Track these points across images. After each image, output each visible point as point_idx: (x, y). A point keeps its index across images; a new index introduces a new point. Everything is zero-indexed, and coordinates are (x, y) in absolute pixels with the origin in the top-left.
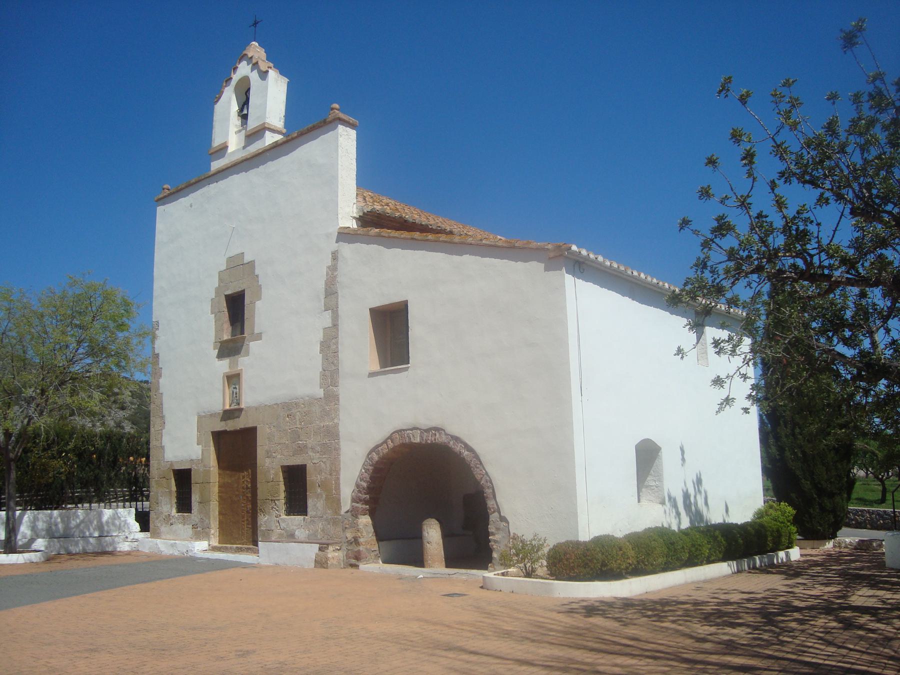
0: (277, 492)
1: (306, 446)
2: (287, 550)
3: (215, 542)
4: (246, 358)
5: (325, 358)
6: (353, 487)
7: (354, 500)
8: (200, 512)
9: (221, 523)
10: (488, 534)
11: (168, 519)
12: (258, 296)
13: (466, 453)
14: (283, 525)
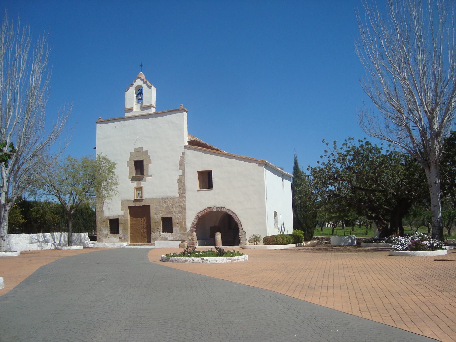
0: (160, 226)
1: (172, 211)
2: (165, 244)
3: (129, 243)
4: (145, 183)
5: (180, 185)
6: (191, 224)
7: (191, 227)
8: (123, 233)
9: (131, 236)
10: (239, 236)
11: (106, 236)
13: (232, 214)
14: (162, 236)
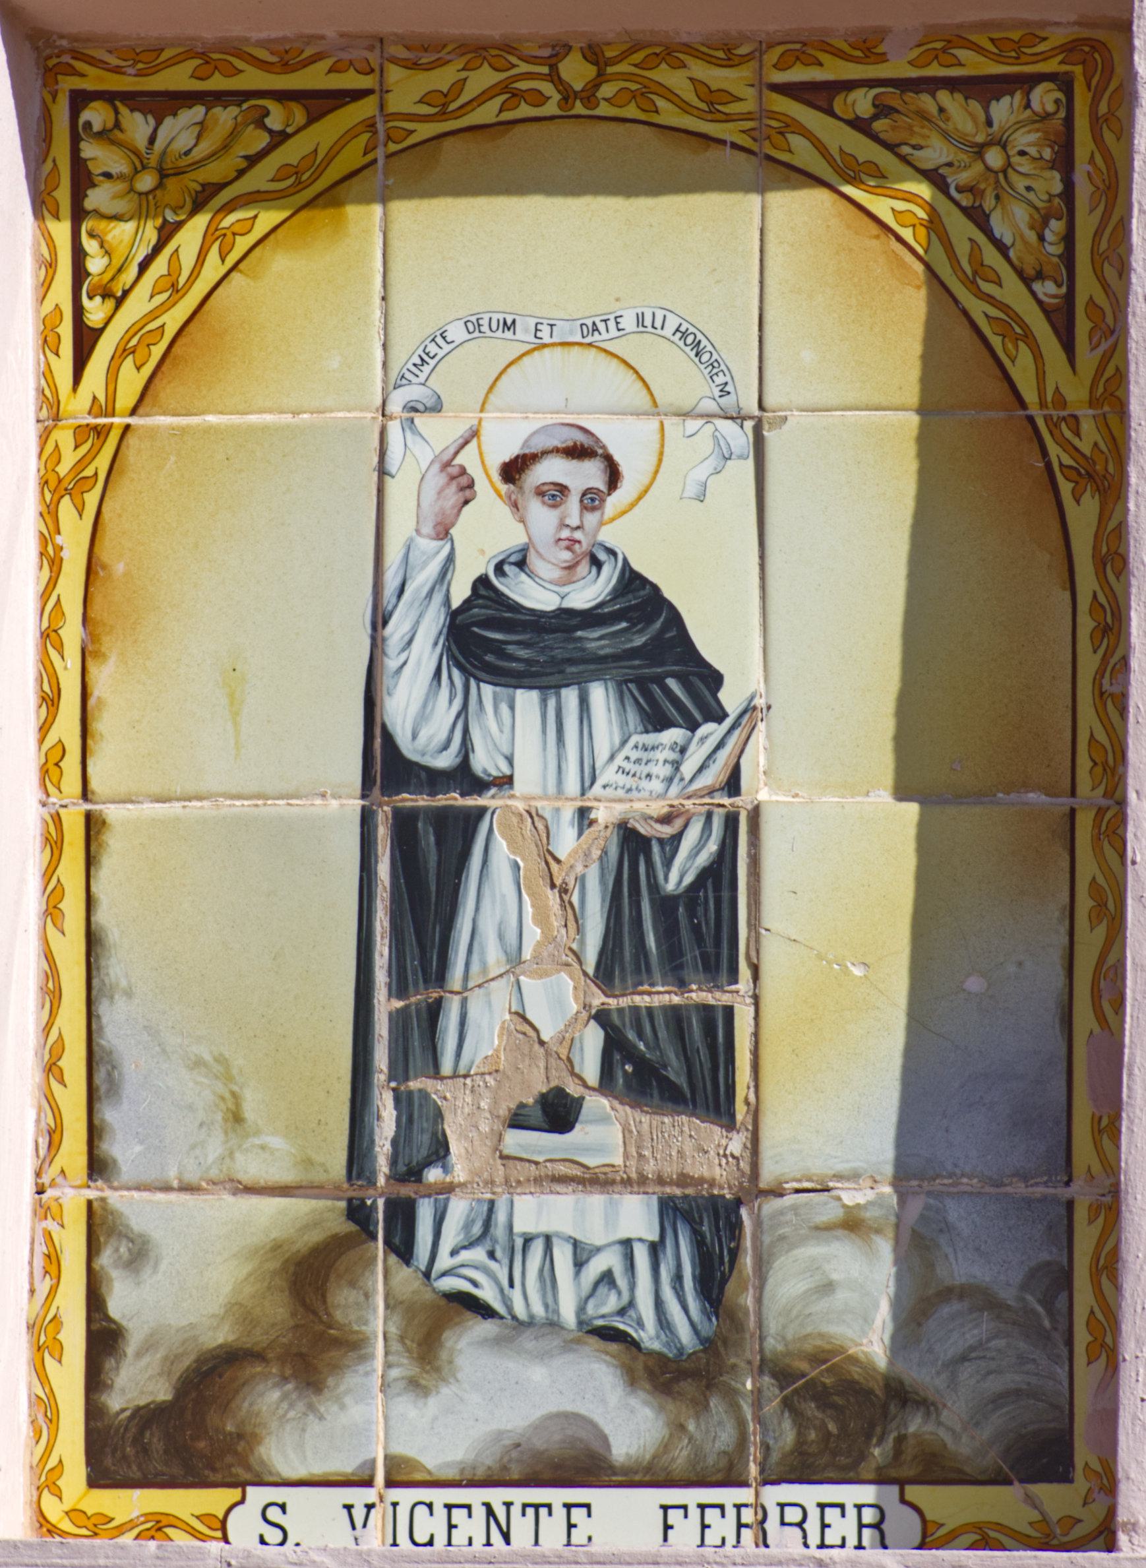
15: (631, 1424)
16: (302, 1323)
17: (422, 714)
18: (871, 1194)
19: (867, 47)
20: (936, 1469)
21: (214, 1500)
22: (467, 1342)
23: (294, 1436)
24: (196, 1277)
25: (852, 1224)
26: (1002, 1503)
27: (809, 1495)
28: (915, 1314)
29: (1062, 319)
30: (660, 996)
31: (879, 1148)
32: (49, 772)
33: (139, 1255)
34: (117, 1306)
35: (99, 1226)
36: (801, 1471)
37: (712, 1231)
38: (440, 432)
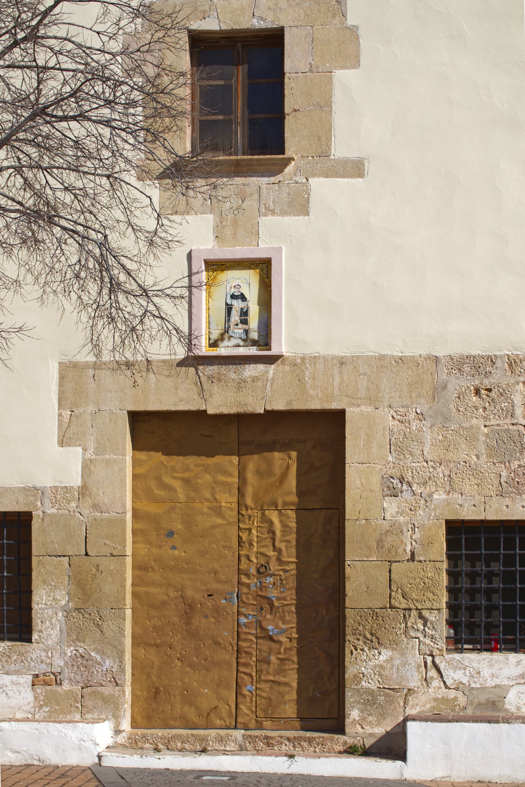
8: (74, 633)
12: (347, 49)
15: (242, 343)
16: (222, 338)
17: (229, 301)
18: (256, 329)
19: (256, 261)
20: (260, 346)
21: (216, 348)
22: (232, 338)
23: (221, 344)
24: (215, 335)
25: (255, 331)
26: (264, 348)
27: (253, 347)
28: (259, 336)
29: (267, 277)
30: (243, 318)
31: (257, 327)
32: (206, 305)
33: (212, 334)
34: (210, 337)
35: (209, 332)
36: (252, 346)
37: (246, 332)
38: (230, 285)
